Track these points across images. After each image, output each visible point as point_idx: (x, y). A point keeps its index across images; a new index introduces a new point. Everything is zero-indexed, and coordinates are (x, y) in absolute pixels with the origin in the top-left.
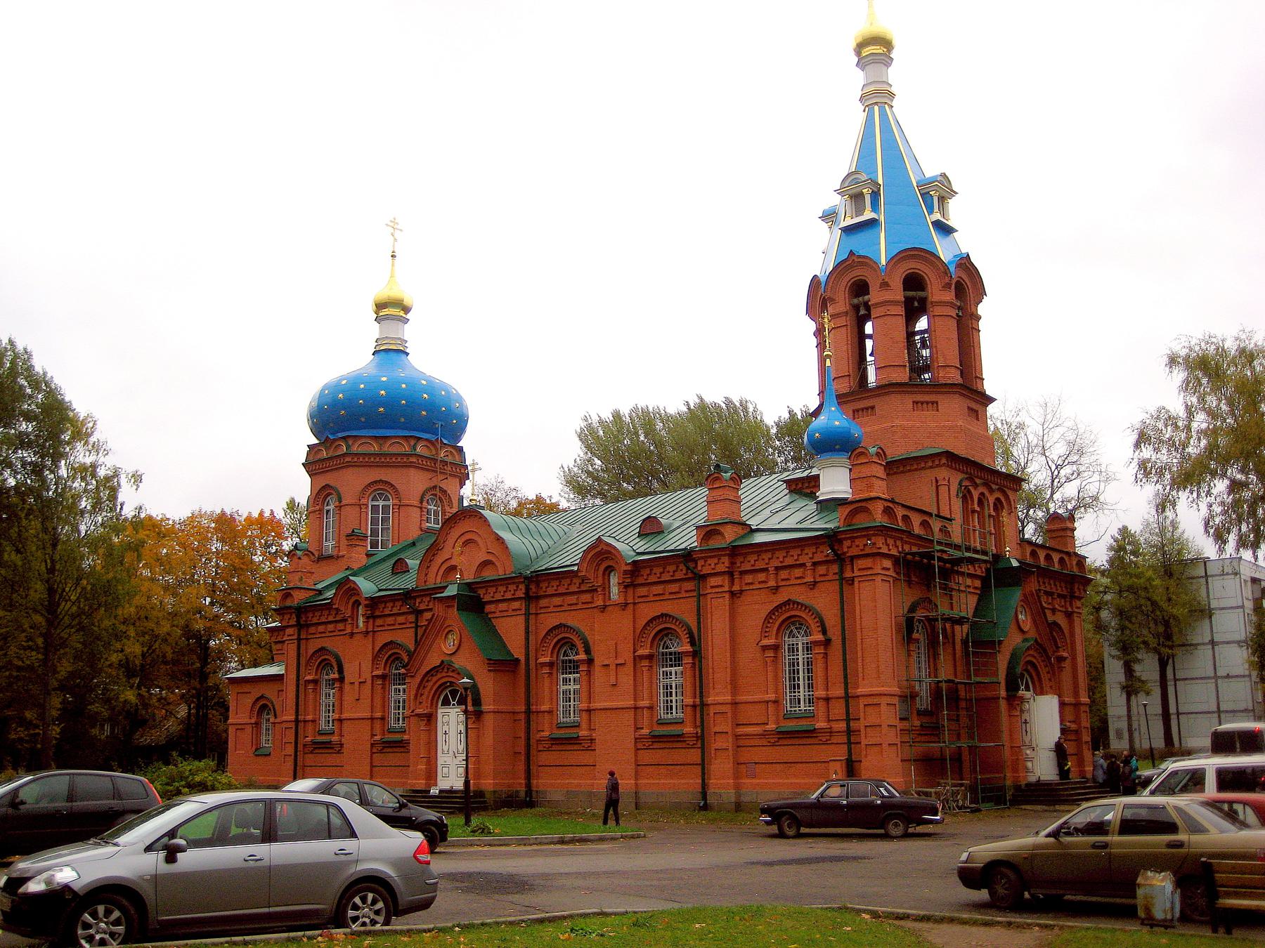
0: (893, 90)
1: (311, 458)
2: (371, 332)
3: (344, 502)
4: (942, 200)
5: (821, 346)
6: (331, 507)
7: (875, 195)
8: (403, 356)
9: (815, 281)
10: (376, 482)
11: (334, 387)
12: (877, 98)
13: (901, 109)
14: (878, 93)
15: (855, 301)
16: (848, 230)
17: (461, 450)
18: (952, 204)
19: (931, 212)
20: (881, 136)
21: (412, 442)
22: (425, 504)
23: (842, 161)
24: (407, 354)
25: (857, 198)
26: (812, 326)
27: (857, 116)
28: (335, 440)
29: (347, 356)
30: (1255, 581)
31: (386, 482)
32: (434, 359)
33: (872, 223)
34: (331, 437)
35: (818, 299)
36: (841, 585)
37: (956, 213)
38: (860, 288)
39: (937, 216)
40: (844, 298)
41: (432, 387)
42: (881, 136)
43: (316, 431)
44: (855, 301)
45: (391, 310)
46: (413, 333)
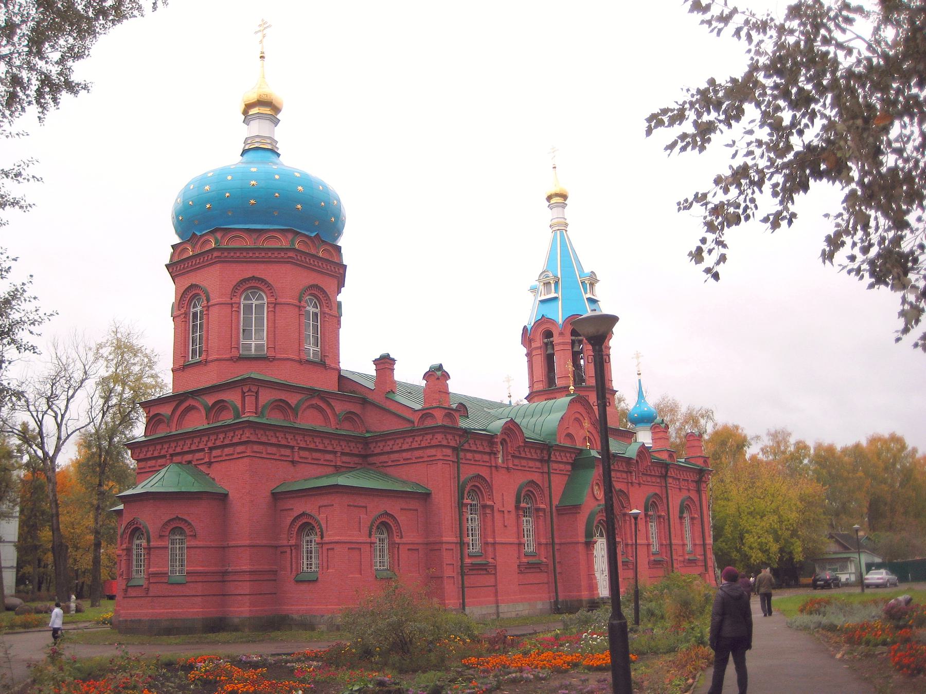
0: (567, 221)
1: (176, 260)
2: (241, 132)
3: (212, 302)
4: (592, 285)
5: (530, 363)
6: (199, 309)
7: (556, 283)
8: (273, 157)
9: (525, 329)
10: (248, 279)
11: (202, 181)
12: (560, 227)
13: (572, 233)
14: (559, 224)
15: (546, 340)
16: (542, 302)
17: (339, 249)
18: (597, 286)
19: (586, 293)
20: (562, 250)
21: (290, 236)
22: (303, 303)
23: (539, 265)
24: (279, 155)
25: (547, 284)
26: (525, 351)
27: (548, 234)
28: (201, 236)
29: (213, 153)
30: (407, 690)
31: (259, 279)
32: (306, 154)
33: (555, 299)
34: (198, 234)
35: (527, 337)
36: (518, 516)
37: (600, 292)
38: (549, 334)
39: (589, 295)
40: (540, 339)
41: (307, 181)
42: (562, 250)
43: (180, 234)
44: (546, 340)
45: (264, 108)
46: (283, 134)
